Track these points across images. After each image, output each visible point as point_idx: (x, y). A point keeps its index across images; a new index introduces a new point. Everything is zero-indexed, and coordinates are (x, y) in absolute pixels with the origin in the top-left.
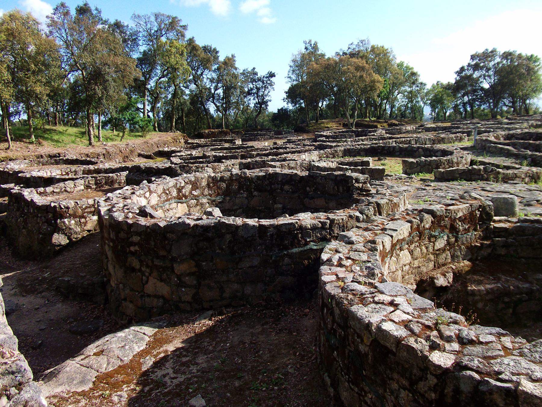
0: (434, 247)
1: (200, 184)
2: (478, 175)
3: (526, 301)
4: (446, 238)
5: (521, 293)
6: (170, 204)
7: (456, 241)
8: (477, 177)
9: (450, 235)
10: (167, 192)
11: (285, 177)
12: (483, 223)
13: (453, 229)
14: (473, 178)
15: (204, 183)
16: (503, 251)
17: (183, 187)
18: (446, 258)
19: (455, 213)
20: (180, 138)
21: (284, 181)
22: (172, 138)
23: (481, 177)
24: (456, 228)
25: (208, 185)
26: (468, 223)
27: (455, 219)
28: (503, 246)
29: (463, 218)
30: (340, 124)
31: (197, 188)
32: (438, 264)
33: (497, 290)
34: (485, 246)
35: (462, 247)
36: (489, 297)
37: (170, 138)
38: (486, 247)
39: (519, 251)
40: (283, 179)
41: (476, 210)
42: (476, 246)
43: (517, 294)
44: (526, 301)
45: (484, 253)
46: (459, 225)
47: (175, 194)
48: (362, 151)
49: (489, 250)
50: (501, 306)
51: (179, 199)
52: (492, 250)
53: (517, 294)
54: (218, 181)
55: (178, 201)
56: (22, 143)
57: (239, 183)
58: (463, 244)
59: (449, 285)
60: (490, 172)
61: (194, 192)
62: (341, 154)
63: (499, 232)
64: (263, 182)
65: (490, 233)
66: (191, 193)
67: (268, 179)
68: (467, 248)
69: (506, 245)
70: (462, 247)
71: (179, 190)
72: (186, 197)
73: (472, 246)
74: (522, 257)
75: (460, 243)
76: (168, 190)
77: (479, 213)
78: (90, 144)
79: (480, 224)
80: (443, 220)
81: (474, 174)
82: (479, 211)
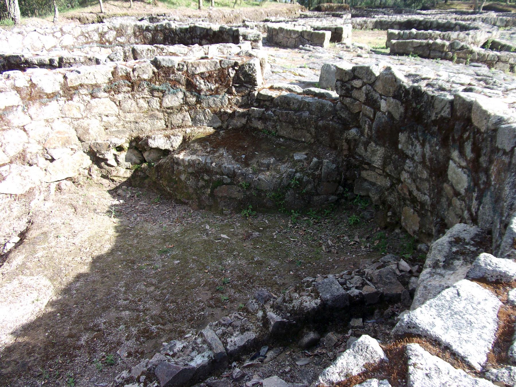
0: (161, 104)
1: (126, 32)
2: (440, 51)
3: (227, 184)
4: (181, 95)
5: (222, 174)
6: (91, 47)
7: (198, 102)
8: (440, 54)
9: (188, 94)
10: (87, 35)
11: (202, 31)
12: (241, 86)
13: (191, 86)
14: (432, 55)
15: (130, 31)
16: (259, 125)
17: (105, 33)
18: (183, 120)
19: (193, 66)
20: (296, 9)
21: (202, 35)
22: (288, 9)
23: (444, 54)
24: (196, 86)
25: (134, 33)
26: (216, 83)
27: (194, 75)
28: (260, 119)
29: (207, 75)
30: (471, 6)
31: (123, 35)
32: (172, 124)
33: (199, 164)
34: (237, 114)
35: (207, 110)
36: (190, 170)
37: (285, 9)
38: (239, 116)
39: (278, 127)
40: (201, 33)
41: (228, 68)
42: (225, 113)
43: (217, 173)
44: (227, 184)
45: (239, 123)
46: (200, 83)
47: (96, 37)
48: (396, 24)
49: (244, 121)
50: (201, 183)
51: (102, 44)
52: (247, 121)
53: (217, 173)
54: (144, 31)
55: (101, 45)
56: (142, 3)
57: (165, 34)
58: (210, 107)
59: (171, 149)
60: (459, 50)
61: (118, 39)
62: (370, 26)
63: (264, 101)
64: (185, 35)
65: (252, 100)
66: (115, 39)
67: (190, 33)
68: (215, 112)
69: (262, 118)
70: (207, 110)
71: (102, 35)
72: (110, 43)
73: (220, 111)
74: (282, 137)
75: (204, 105)
76: (88, 33)
77: (234, 72)
78: (199, 8)
79: (235, 87)
80: (173, 73)
81: (434, 50)
82: (234, 69)
